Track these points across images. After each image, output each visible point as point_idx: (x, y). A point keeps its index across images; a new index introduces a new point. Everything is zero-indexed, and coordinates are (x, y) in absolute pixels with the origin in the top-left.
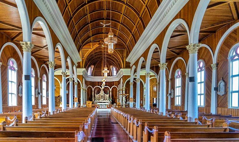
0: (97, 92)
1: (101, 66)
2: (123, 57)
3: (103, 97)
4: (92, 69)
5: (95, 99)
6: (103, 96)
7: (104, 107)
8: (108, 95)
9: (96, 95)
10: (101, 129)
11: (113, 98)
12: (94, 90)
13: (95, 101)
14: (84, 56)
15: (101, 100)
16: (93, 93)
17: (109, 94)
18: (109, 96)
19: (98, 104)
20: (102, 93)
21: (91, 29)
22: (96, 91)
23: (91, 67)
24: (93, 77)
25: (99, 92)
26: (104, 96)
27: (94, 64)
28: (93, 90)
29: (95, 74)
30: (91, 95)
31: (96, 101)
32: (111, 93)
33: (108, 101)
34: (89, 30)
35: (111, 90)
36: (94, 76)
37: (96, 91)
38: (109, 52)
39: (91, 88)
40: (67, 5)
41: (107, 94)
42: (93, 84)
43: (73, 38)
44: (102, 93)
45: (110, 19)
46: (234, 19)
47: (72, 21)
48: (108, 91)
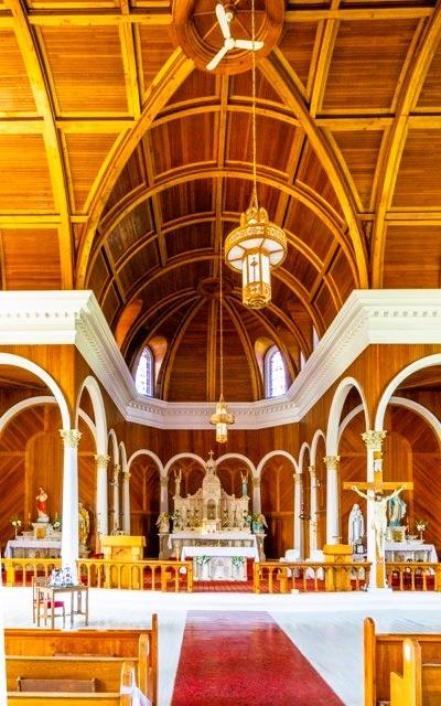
0: (183, 482)
1: (205, 345)
2: (366, 204)
3: (217, 510)
4: (158, 366)
5: (171, 522)
6: (217, 502)
7: (226, 571)
8: (243, 503)
9: (177, 500)
10: (411, 251)
11: (269, 520)
12: (171, 475)
13: (171, 531)
14: (79, 203)
15: (207, 530)
16: (164, 490)
17: (250, 492)
18: (251, 504)
19: (188, 551)
20: (211, 489)
21: (163, 229)
22: (178, 481)
23: (152, 351)
24: (163, 404)
25: (192, 484)
26: (221, 509)
27: (168, 333)
28: (164, 472)
29: (173, 388)
30: (155, 505)
31: (177, 534)
32: (257, 491)
33: (246, 534)
34: (155, 233)
35: (257, 473)
36: (169, 400)
37: (178, 481)
38: (245, 301)
39: (153, 462)
40: (112, 275)
41: (239, 496)
42: (165, 442)
43: (106, 312)
44: (211, 489)
45: (251, 168)
46: (335, 569)
47: (103, 249)
48: (244, 481)
